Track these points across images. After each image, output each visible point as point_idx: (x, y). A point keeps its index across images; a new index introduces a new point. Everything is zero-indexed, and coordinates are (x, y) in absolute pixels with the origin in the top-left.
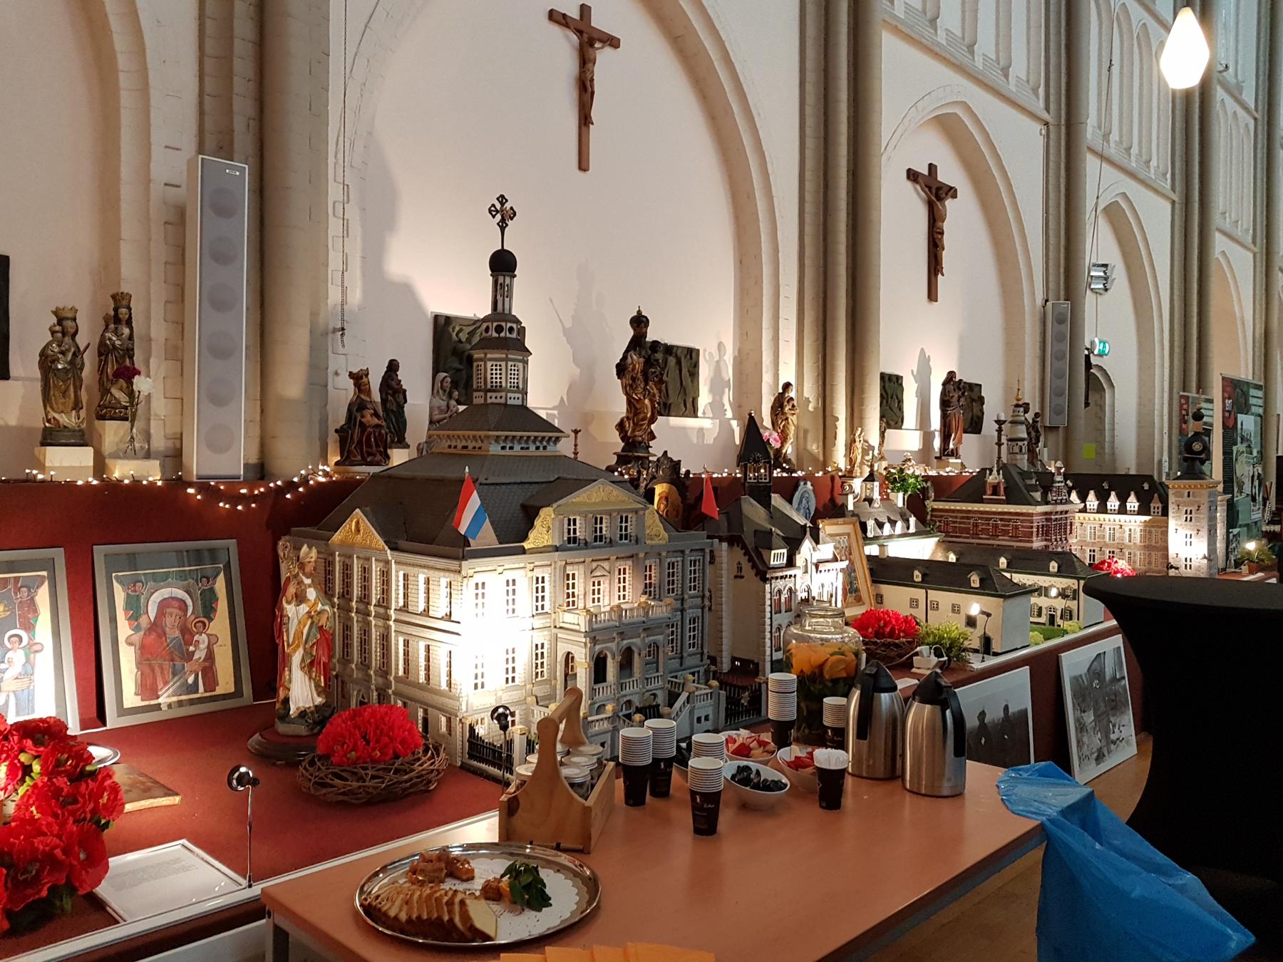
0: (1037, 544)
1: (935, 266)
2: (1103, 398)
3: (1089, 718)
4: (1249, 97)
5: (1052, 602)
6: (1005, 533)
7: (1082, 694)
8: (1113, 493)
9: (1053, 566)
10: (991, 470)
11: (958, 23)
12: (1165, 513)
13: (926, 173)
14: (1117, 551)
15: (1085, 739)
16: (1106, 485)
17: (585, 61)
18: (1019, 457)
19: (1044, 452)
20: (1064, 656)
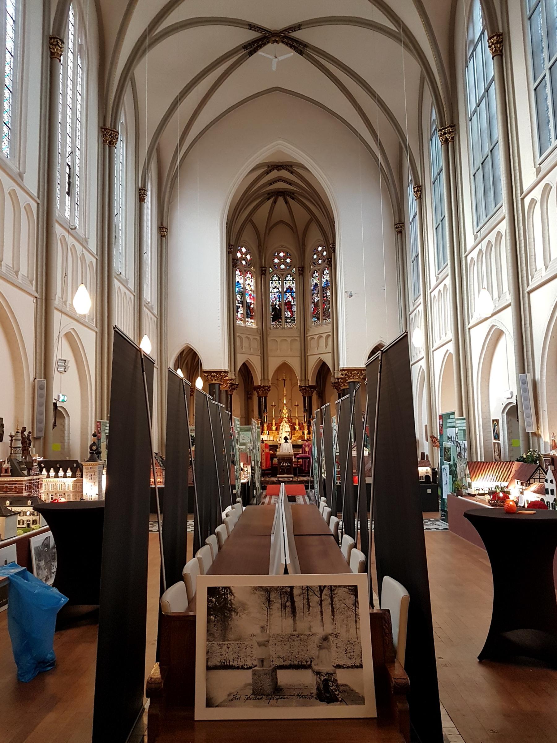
0: (25, 494)
2: (64, 421)
3: (42, 563)
4: (131, 286)
5: (28, 518)
6: (11, 490)
7: (39, 554)
8: (61, 469)
9: (29, 503)
10: (4, 462)
12: (82, 477)
14: (63, 494)
15: (40, 572)
16: (58, 466)
18: (18, 455)
19: (33, 449)
20: (32, 539)
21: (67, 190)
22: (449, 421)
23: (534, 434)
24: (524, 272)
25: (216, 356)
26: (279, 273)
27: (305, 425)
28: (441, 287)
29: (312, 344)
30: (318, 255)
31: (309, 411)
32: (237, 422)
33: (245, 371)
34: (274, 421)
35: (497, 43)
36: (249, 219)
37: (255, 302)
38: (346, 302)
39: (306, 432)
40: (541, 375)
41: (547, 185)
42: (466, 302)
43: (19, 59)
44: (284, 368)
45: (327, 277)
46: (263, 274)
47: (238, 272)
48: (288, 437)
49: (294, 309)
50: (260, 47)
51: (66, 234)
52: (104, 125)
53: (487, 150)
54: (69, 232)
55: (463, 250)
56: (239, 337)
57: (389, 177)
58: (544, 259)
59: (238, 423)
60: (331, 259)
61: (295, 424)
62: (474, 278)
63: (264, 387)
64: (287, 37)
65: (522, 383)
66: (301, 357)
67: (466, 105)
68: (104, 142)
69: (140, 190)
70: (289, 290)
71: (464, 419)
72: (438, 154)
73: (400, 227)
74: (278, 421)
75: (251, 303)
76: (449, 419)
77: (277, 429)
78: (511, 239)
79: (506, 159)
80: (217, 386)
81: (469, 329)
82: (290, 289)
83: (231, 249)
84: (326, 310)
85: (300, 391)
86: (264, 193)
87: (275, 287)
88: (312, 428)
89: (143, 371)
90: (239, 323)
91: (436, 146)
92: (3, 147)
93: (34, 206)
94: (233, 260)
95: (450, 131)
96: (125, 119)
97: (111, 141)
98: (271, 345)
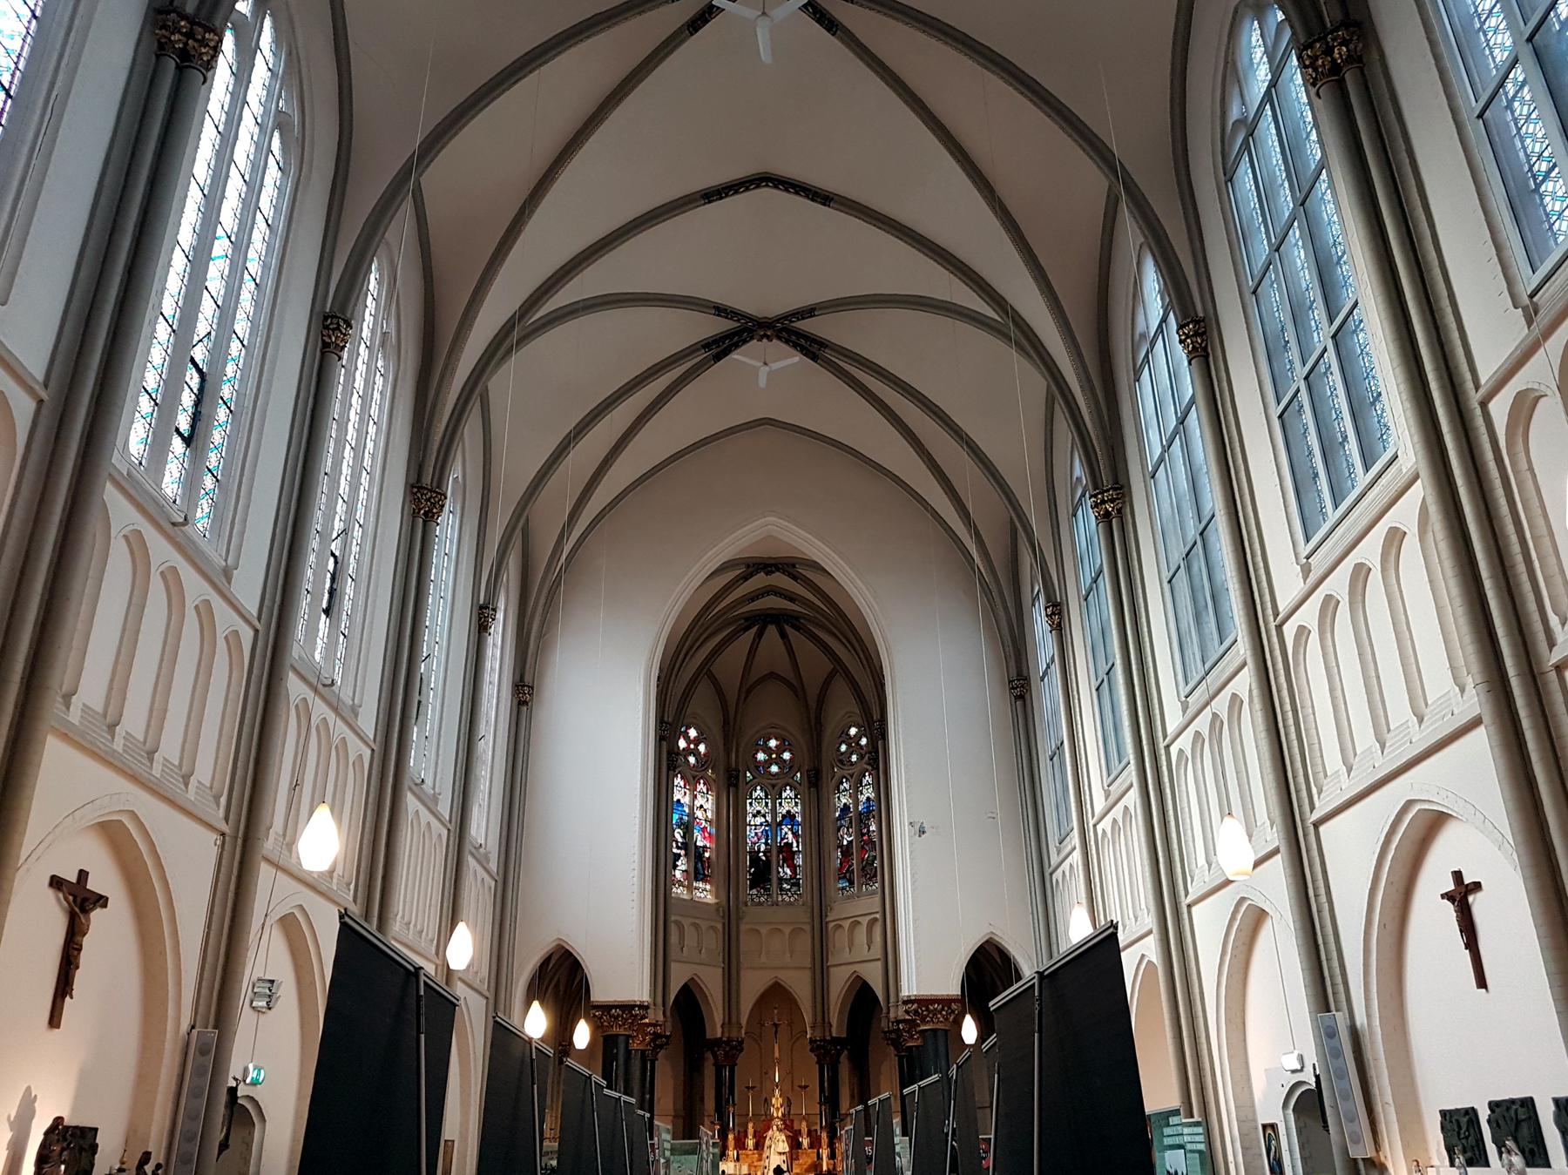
1: (64, 986)
2: (251, 1134)
4: (444, 808)
11: (142, 728)
13: (74, 879)
17: (1346, 13)
21: (324, 605)
22: (1167, 1131)
23: (1370, 1162)
24: (1301, 779)
25: (622, 971)
26: (766, 782)
27: (824, 1135)
28: (1117, 812)
29: (839, 939)
30: (849, 745)
31: (830, 1100)
32: (664, 1135)
33: (688, 1004)
34: (750, 1125)
35: (1196, 334)
36: (705, 671)
38: (911, 844)
39: (825, 1153)
40: (1369, 1016)
41: (1328, 598)
42: (1175, 846)
43: (257, 352)
44: (776, 994)
45: (868, 792)
46: (731, 784)
47: (678, 781)
48: (784, 1167)
49: (799, 861)
50: (736, 346)
51: (310, 695)
52: (419, 480)
53: (1192, 532)
54: (316, 691)
55: (1160, 734)
56: (678, 923)
57: (993, 587)
58: (1342, 750)
59: (668, 1137)
60: (877, 752)
61: (799, 1133)
62: (1192, 793)
63: (730, 1040)
64: (786, 330)
65: (1326, 1035)
67: (1142, 450)
68: (415, 514)
69: (481, 608)
71: (1197, 1124)
72: (1090, 542)
73: (1019, 687)
74: (760, 1127)
75: (705, 847)
76: (1168, 1125)
77: (759, 1146)
78: (1264, 709)
79: (1236, 550)
80: (621, 1039)
81: (1189, 906)
82: (789, 816)
83: (666, 729)
84: (869, 863)
86: (737, 618)
87: (757, 811)
88: (841, 1147)
89: (419, 1033)
90: (678, 891)
91: (1087, 525)
92: (199, 515)
93: (247, 635)
94: (669, 753)
95: (1113, 496)
96: (460, 473)
97: (431, 510)
98: (746, 943)
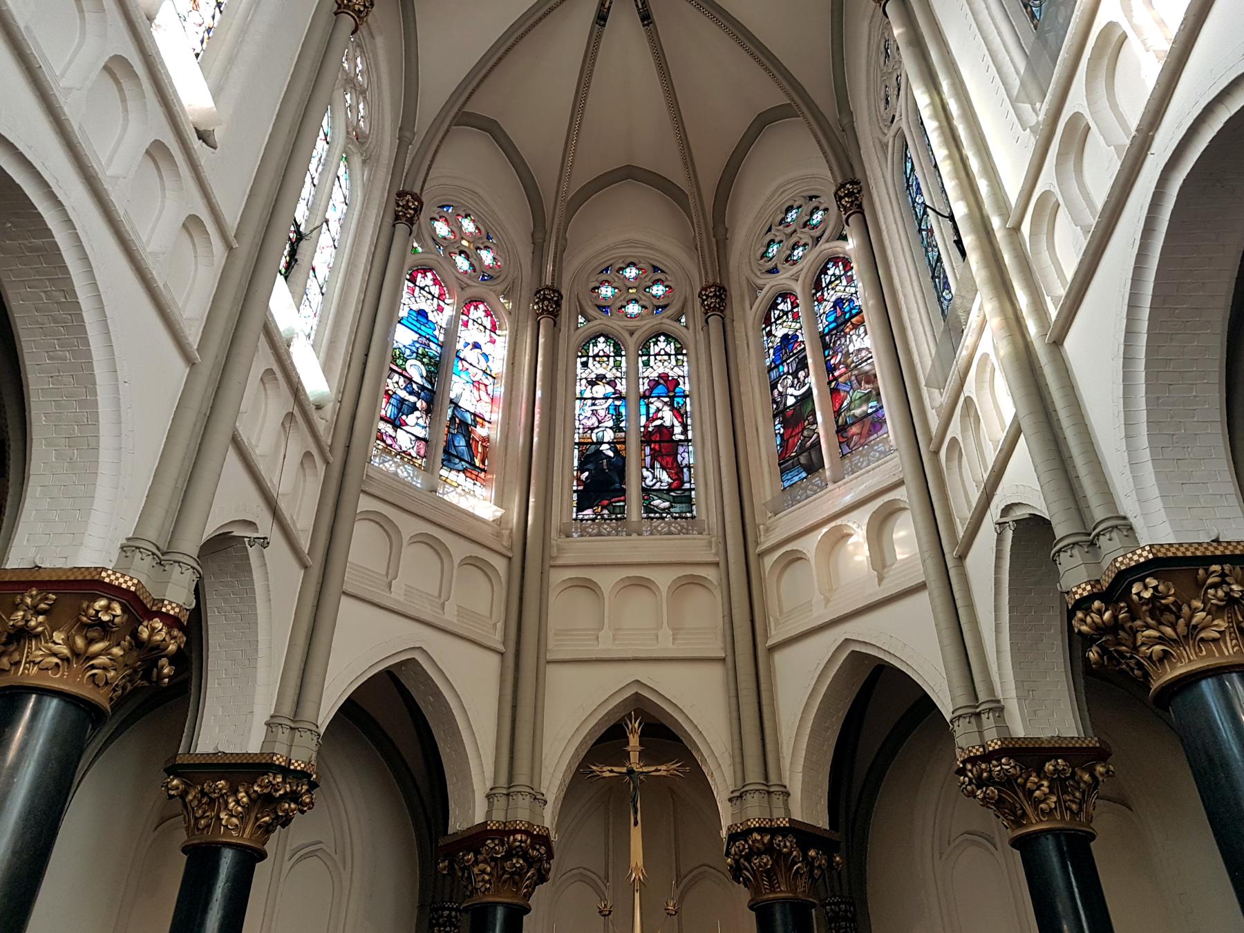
37: (497, 416)
44: (641, 736)
46: (548, 306)
49: (686, 457)
63: (503, 833)
66: (728, 661)
70: (661, 389)
85: (736, 872)
